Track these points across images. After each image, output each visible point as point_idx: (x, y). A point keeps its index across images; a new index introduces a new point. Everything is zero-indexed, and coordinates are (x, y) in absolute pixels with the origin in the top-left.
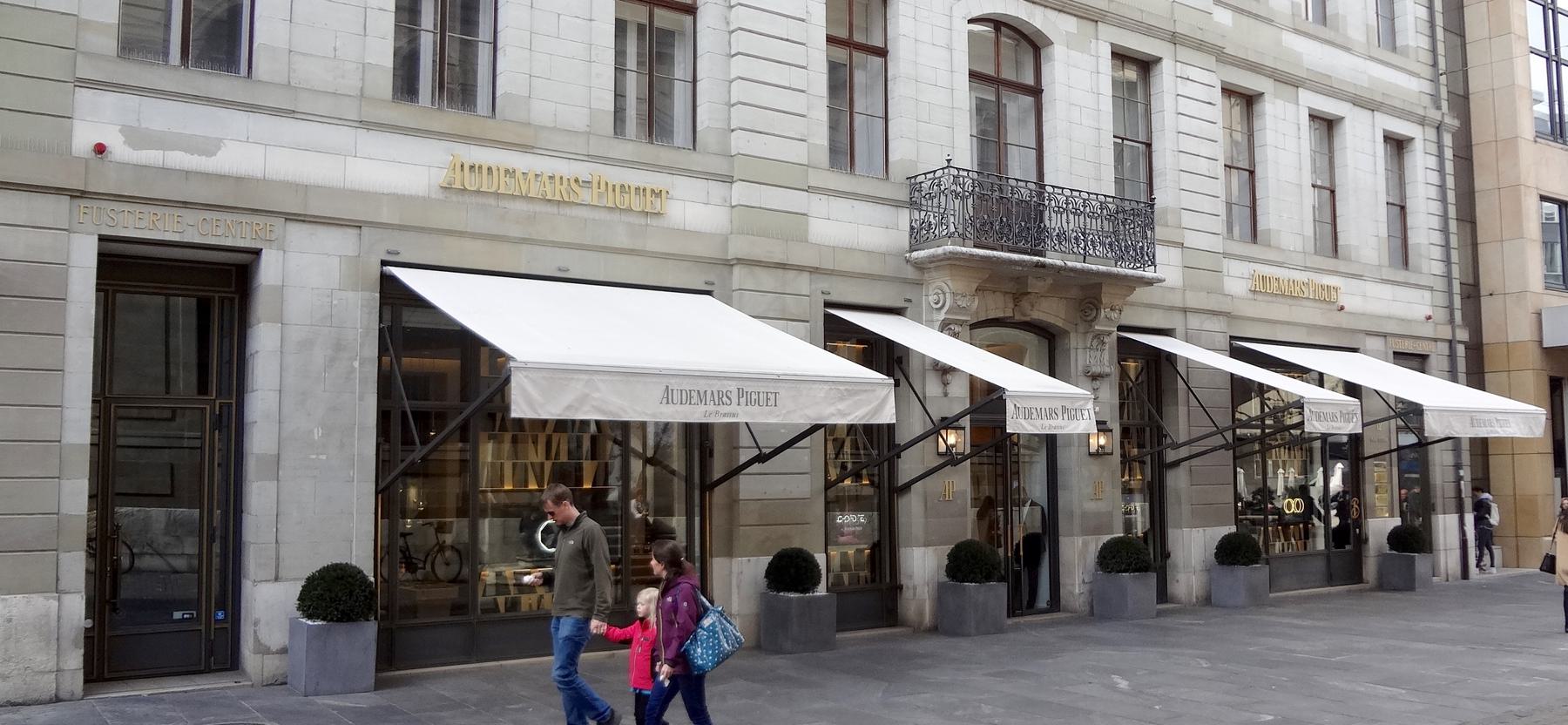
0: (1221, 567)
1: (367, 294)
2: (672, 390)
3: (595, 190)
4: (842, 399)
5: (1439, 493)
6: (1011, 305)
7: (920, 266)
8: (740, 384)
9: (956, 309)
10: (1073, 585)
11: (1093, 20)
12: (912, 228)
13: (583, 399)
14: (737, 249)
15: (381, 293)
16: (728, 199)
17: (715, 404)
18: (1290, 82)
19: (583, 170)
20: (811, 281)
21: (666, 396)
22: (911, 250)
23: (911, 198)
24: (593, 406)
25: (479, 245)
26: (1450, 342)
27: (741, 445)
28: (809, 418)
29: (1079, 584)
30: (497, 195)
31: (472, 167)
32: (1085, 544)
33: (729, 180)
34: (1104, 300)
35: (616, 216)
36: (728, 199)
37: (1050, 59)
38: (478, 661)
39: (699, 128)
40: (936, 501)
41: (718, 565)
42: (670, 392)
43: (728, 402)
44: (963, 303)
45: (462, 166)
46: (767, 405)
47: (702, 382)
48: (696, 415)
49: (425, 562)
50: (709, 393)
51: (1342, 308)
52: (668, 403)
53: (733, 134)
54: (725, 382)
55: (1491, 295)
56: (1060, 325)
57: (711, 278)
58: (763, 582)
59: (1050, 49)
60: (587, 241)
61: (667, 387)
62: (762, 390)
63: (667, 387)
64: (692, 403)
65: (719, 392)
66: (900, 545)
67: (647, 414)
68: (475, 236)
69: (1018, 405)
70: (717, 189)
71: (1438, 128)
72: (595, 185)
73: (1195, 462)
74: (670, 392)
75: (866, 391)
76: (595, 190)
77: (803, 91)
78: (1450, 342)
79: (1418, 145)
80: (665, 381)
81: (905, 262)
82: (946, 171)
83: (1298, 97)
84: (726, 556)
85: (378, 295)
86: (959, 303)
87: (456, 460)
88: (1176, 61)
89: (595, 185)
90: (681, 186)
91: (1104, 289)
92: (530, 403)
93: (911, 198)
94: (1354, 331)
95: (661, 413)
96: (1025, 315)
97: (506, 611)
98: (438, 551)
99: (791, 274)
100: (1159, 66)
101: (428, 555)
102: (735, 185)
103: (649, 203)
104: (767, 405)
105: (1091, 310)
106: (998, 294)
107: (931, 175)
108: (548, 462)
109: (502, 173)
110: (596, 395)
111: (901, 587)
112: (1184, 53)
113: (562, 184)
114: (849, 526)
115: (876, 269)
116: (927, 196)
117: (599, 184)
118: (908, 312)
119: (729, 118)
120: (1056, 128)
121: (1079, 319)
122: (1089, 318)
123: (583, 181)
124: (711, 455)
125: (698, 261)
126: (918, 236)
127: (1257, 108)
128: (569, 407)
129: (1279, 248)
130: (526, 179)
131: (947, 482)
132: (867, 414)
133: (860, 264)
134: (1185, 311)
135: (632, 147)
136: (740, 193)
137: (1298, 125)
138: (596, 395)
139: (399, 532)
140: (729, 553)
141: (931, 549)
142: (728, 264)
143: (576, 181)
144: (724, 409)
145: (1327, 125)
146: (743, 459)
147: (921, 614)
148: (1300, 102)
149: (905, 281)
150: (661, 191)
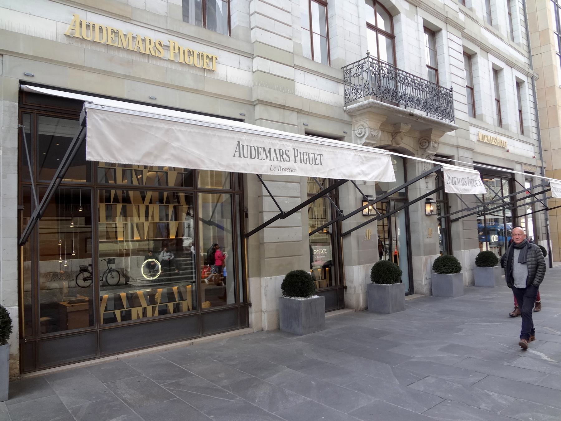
0: (478, 268)
1: (8, 103)
2: (243, 146)
3: (172, 51)
4: (362, 163)
5: (541, 231)
6: (391, 139)
7: (351, 114)
8: (296, 145)
9: (371, 137)
10: (421, 281)
12: (346, 94)
13: (164, 146)
14: (259, 94)
15: (19, 103)
16: (251, 68)
17: (277, 160)
18: (487, 50)
19: (165, 38)
20: (298, 118)
21: (238, 150)
22: (346, 106)
23: (345, 78)
24: (172, 155)
25: (93, 77)
26: (541, 167)
27: (264, 210)
28: (344, 175)
29: (424, 280)
30: (107, 46)
31: (88, 26)
32: (426, 260)
33: (251, 56)
34: (432, 138)
35: (185, 69)
36: (251, 68)
37: (399, 21)
38: (102, 356)
39: (233, 27)
40: (363, 241)
41: (252, 282)
42: (241, 147)
43: (288, 159)
44: (374, 133)
45: (81, 24)
46: (315, 164)
47: (267, 141)
48: (264, 168)
49: (103, 278)
50: (272, 151)
51: (508, 151)
52: (240, 156)
53: (252, 31)
54: (285, 143)
55: (545, 151)
56: (411, 151)
57: (243, 112)
58: (281, 291)
59: (398, 16)
60: (168, 81)
61: (239, 142)
62: (311, 151)
63: (239, 142)
64: (260, 158)
65: (280, 150)
66: (345, 265)
67: (222, 165)
68: (92, 70)
69: (449, 176)
70: (244, 61)
71: (532, 78)
72: (172, 48)
73: (464, 219)
74: (241, 147)
75: (376, 158)
76: (172, 51)
77: (289, 12)
78: (541, 167)
79: (526, 84)
80: (236, 136)
81: (343, 112)
82: (366, 60)
83: (488, 57)
84: (258, 276)
85: (17, 104)
86: (373, 133)
87: (114, 232)
88: (447, 31)
89: (172, 48)
90: (224, 56)
91: (433, 132)
92: (107, 147)
93: (345, 78)
94: (512, 161)
95: (234, 165)
96: (398, 144)
97: (122, 321)
98: (109, 272)
99: (288, 113)
100: (440, 33)
101: (104, 274)
102: (254, 60)
103: (205, 64)
104: (315, 164)
105: (426, 143)
106: (385, 132)
107: (357, 64)
108: (147, 222)
109: (109, 31)
110: (175, 144)
111: (346, 288)
112: (450, 28)
113: (150, 44)
114: (319, 256)
115: (330, 113)
116: (355, 75)
117: (174, 48)
118: (346, 138)
119: (250, 22)
120: (403, 54)
121: (419, 147)
122: (424, 147)
123: (164, 45)
124: (247, 217)
125: (235, 100)
126: (348, 100)
127: (473, 60)
128: (148, 154)
129: (485, 122)
130: (126, 39)
131: (367, 230)
132: (379, 175)
133: (323, 111)
134: (458, 147)
135: (192, 28)
136: (258, 64)
137: (489, 69)
138: (175, 144)
139: (551, 180)
140: (259, 274)
141: (362, 266)
142: (253, 104)
143: (160, 44)
144: (285, 165)
145: (497, 72)
146: (266, 219)
147: (358, 301)
148: (489, 59)
149: (343, 122)
150: (212, 57)
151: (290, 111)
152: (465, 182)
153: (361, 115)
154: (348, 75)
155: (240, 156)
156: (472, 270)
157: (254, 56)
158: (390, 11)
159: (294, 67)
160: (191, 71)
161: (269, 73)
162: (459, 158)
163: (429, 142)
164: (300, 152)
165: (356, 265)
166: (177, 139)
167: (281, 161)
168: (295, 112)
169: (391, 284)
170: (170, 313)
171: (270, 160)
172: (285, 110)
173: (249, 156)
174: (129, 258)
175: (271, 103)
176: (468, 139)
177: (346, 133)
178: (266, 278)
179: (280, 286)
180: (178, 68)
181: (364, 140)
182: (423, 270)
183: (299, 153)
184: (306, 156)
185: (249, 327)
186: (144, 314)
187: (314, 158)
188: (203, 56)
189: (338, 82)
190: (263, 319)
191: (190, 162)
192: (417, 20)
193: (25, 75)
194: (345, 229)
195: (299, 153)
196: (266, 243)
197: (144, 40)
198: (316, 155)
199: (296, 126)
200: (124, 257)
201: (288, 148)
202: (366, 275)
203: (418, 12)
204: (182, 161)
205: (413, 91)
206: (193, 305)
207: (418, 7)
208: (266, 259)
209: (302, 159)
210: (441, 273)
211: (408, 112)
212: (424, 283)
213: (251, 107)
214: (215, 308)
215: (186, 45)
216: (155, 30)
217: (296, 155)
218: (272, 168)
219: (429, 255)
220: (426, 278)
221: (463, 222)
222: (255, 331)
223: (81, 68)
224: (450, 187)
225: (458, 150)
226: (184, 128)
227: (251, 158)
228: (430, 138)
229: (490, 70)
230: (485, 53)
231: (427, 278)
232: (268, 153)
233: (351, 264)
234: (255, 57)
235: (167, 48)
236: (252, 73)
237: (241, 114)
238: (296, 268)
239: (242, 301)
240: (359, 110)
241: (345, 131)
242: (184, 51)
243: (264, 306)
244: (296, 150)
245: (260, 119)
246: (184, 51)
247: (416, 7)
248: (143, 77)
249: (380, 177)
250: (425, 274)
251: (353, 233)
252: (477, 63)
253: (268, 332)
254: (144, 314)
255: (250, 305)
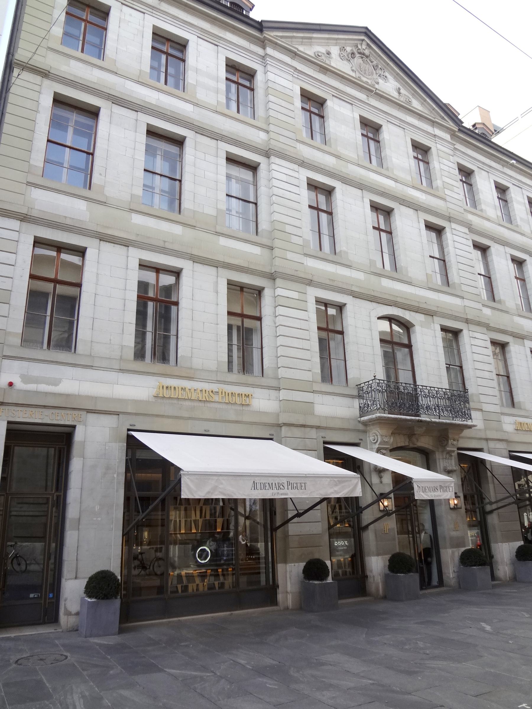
1: (121, 444)
2: (256, 483)
4: (336, 485)
6: (408, 440)
7: (365, 424)
8: (288, 479)
10: (449, 574)
11: (431, 315)
12: (360, 407)
13: (215, 488)
17: (277, 489)
19: (215, 387)
21: (253, 486)
22: (361, 417)
24: (220, 492)
28: (321, 494)
29: (452, 573)
31: (167, 387)
32: (453, 553)
33: (278, 389)
35: (229, 407)
37: (414, 332)
41: (280, 567)
44: (386, 440)
46: (301, 489)
47: (270, 479)
50: (274, 484)
52: (254, 489)
53: (279, 369)
54: (281, 479)
56: (431, 449)
57: (272, 433)
58: (302, 575)
61: (254, 482)
62: (298, 482)
63: (254, 482)
68: (168, 417)
69: (419, 486)
70: (273, 393)
72: (220, 393)
73: (500, 510)
74: (255, 484)
75: (347, 481)
80: (253, 479)
83: (524, 343)
85: (125, 444)
88: (469, 331)
89: (220, 393)
90: (257, 392)
91: (450, 431)
93: (359, 394)
96: (415, 444)
100: (462, 333)
107: (367, 383)
109: (180, 389)
110: (221, 486)
111: (367, 577)
112: (472, 327)
115: (346, 426)
116: (366, 393)
117: (222, 392)
118: (361, 444)
124: (275, 514)
125: (265, 425)
126: (363, 411)
127: (507, 349)
128: (209, 492)
130: (190, 392)
131: (385, 524)
133: (338, 424)
134: (487, 440)
135: (235, 377)
136: (283, 394)
138: (221, 486)
142: (279, 426)
143: (212, 392)
147: (378, 590)
148: (526, 346)
149: (359, 431)
151: (310, 428)
152: (436, 489)
153: (373, 424)
154: (361, 392)
155: (254, 489)
156: (513, 563)
157: (281, 389)
158: (406, 324)
159: (313, 392)
160: (234, 407)
161: (292, 401)
162: (489, 450)
163: (448, 440)
164: (291, 483)
165: (374, 555)
166: (222, 484)
167: (279, 489)
168: (313, 428)
169: (403, 573)
170: (215, 589)
171: (272, 489)
172: (306, 428)
173: (260, 489)
174: (177, 546)
175: (294, 424)
176: (502, 430)
177: (362, 440)
178: (290, 564)
179: (302, 571)
180: (224, 406)
181: (377, 446)
182: (450, 563)
183: (290, 484)
184: (295, 485)
185: (277, 605)
186: (197, 590)
187: (300, 486)
188: (242, 395)
189: (353, 398)
190: (288, 599)
191: (228, 495)
192: (434, 327)
193: (131, 425)
194: (364, 523)
195: (290, 484)
196: (290, 536)
197: (201, 391)
198: (302, 484)
199: (316, 439)
200: (172, 546)
201: (283, 482)
202: (385, 566)
203: (434, 320)
204: (224, 495)
205: (422, 399)
206: (233, 585)
207: (434, 316)
208: (290, 549)
209: (292, 487)
210: (467, 566)
211: (416, 420)
212: (451, 576)
213: (279, 428)
214: (250, 588)
215: (230, 389)
216: (209, 382)
217: (289, 485)
218: (274, 494)
219: (456, 548)
220: (454, 571)
221: (498, 515)
222: (282, 608)
223: (162, 416)
224: (419, 494)
225: (488, 442)
226: (225, 478)
227: (261, 489)
228: (448, 437)
229: (528, 356)
230: (522, 340)
231: (455, 571)
232: (271, 486)
233: (369, 555)
234: (281, 389)
235: (217, 393)
236: (278, 402)
237: (270, 435)
238: (317, 556)
239: (271, 583)
240: (370, 422)
241: (361, 438)
242: (228, 393)
243: (289, 589)
244: (288, 482)
245: (285, 437)
246: (228, 393)
247: (433, 316)
248: (201, 417)
249: (349, 494)
250: (452, 566)
251: (371, 527)
252: (510, 351)
253: (292, 610)
254: (197, 590)
255: (278, 586)
